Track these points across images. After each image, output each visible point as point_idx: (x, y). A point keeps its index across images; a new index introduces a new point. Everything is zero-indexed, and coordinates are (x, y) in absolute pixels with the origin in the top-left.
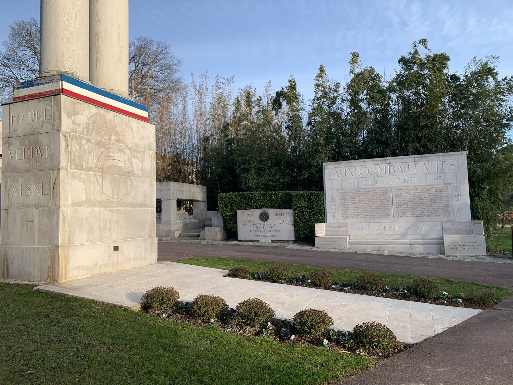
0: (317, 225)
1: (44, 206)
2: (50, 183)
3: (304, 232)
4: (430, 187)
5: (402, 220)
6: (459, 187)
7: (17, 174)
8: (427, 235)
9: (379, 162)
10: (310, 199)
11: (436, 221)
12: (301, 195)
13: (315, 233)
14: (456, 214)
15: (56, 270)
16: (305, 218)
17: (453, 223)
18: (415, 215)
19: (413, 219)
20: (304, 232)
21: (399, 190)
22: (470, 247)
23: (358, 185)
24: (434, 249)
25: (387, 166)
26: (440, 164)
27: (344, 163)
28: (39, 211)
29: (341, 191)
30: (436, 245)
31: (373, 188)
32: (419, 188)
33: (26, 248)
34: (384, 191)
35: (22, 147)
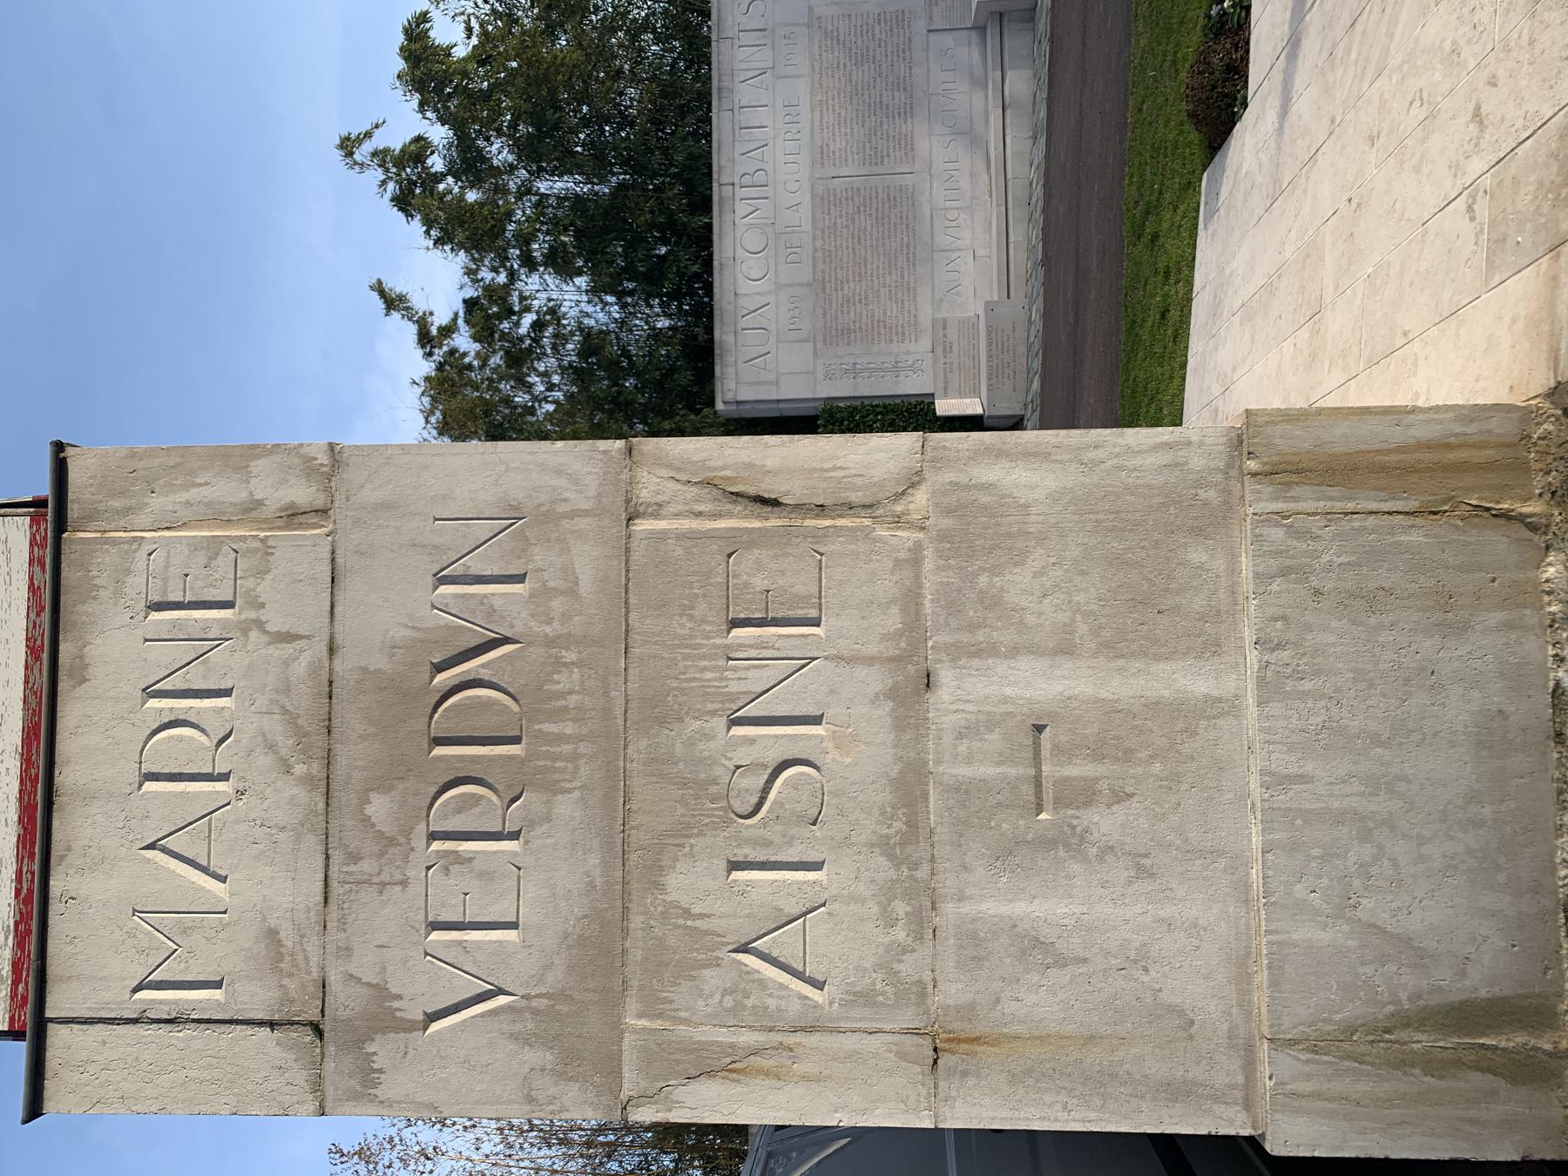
0: (938, 413)
1: (910, 600)
2: (733, 545)
5: (922, 145)
7: (637, 921)
15: (1421, 433)
18: (908, 111)
21: (821, 155)
24: (1017, 42)
26: (746, 38)
27: (722, 335)
28: (957, 653)
30: (1005, 32)
31: (814, 239)
33: (1276, 781)
34: (824, 201)
35: (415, 872)
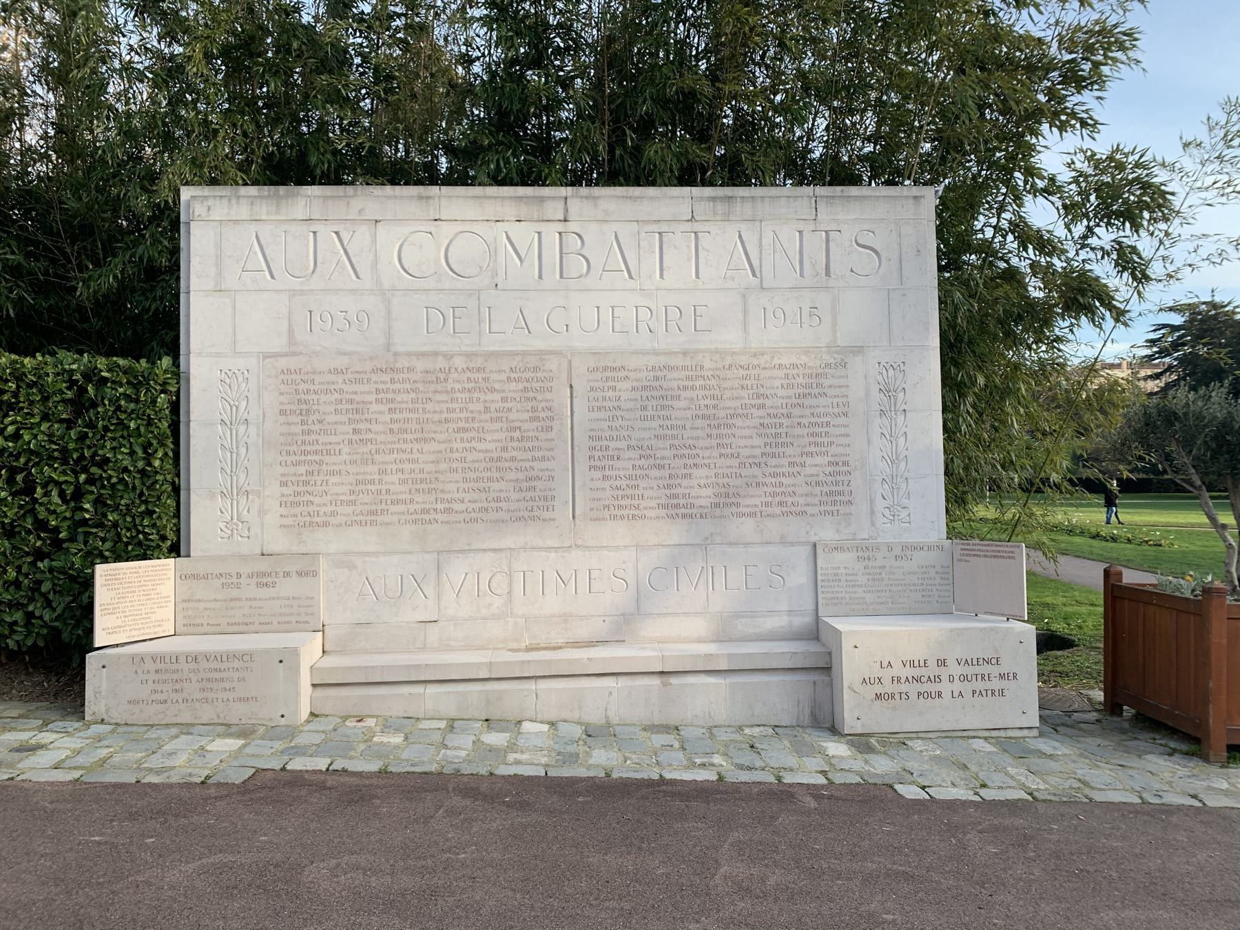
3: (30, 616)
4: (762, 361)
6: (899, 368)
8: (738, 615)
9: (510, 210)
10: (80, 404)
11: (783, 542)
12: (19, 377)
13: (90, 631)
14: (880, 504)
16: (41, 525)
17: (865, 550)
18: (677, 508)
19: (675, 533)
20: (30, 616)
22: (967, 688)
23: (389, 333)
24: (779, 699)
25: (551, 233)
26: (815, 243)
29: (283, 363)
30: (789, 677)
31: (469, 356)
32: (708, 364)
34: (531, 373)
